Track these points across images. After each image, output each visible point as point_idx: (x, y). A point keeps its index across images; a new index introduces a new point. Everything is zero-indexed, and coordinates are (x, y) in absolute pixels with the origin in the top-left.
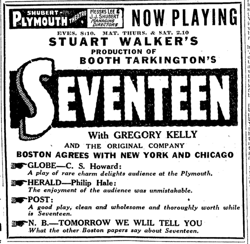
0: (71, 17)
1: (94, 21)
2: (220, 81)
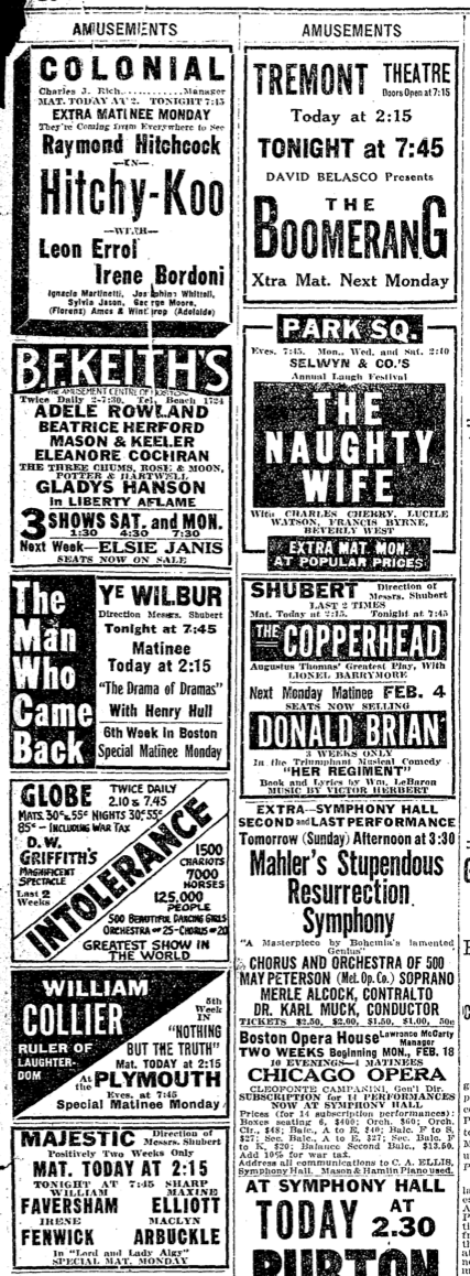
2: (273, 458)
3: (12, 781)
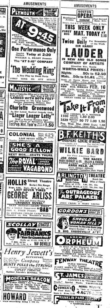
0: (37, 12)
1: (46, 13)
3: (103, 206)
